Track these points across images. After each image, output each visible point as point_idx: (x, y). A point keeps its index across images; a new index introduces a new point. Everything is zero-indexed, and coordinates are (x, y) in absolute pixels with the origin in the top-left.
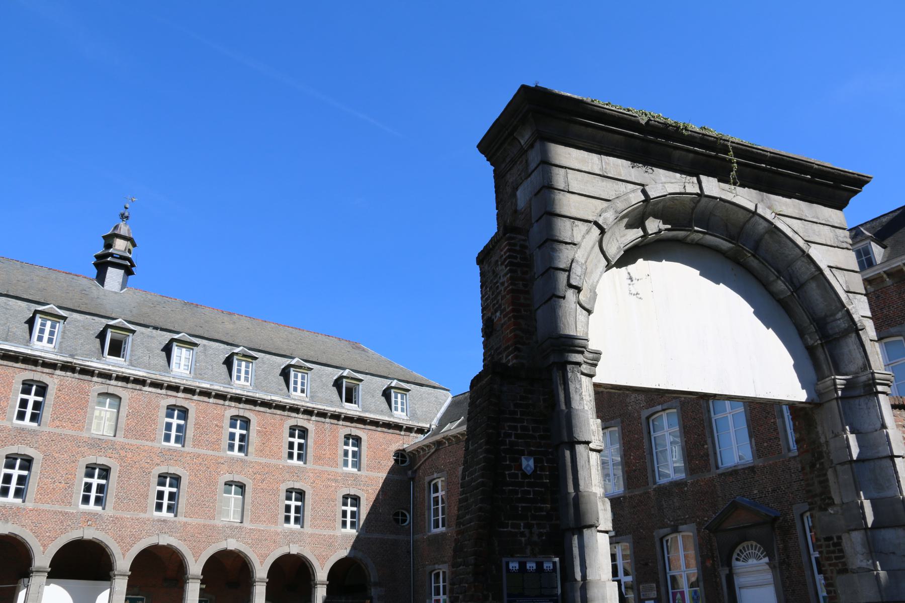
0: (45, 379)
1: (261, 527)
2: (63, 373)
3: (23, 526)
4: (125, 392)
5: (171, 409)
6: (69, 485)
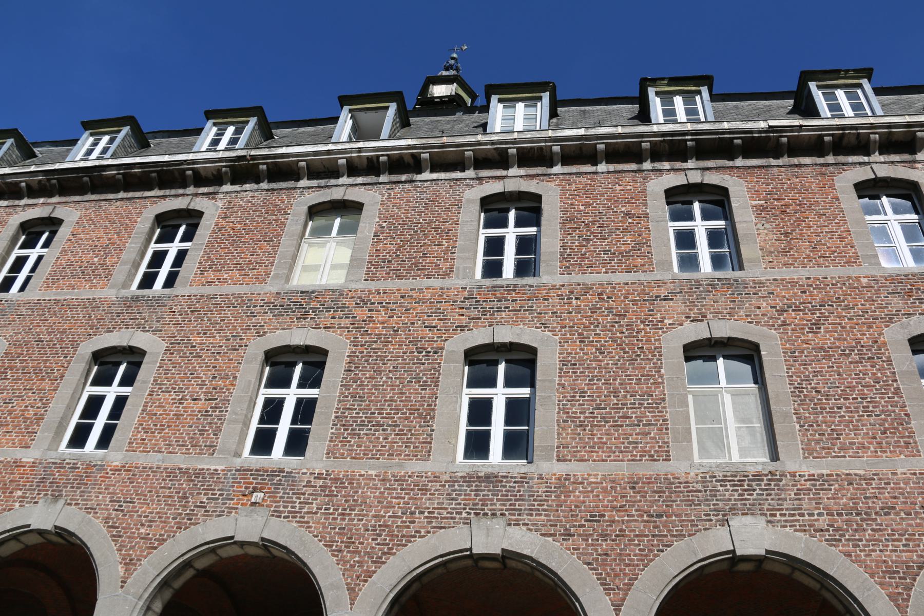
0: (198, 204)
1: (858, 467)
2: (237, 188)
3: (89, 510)
4: (369, 195)
5: (679, 199)
6: (217, 403)
